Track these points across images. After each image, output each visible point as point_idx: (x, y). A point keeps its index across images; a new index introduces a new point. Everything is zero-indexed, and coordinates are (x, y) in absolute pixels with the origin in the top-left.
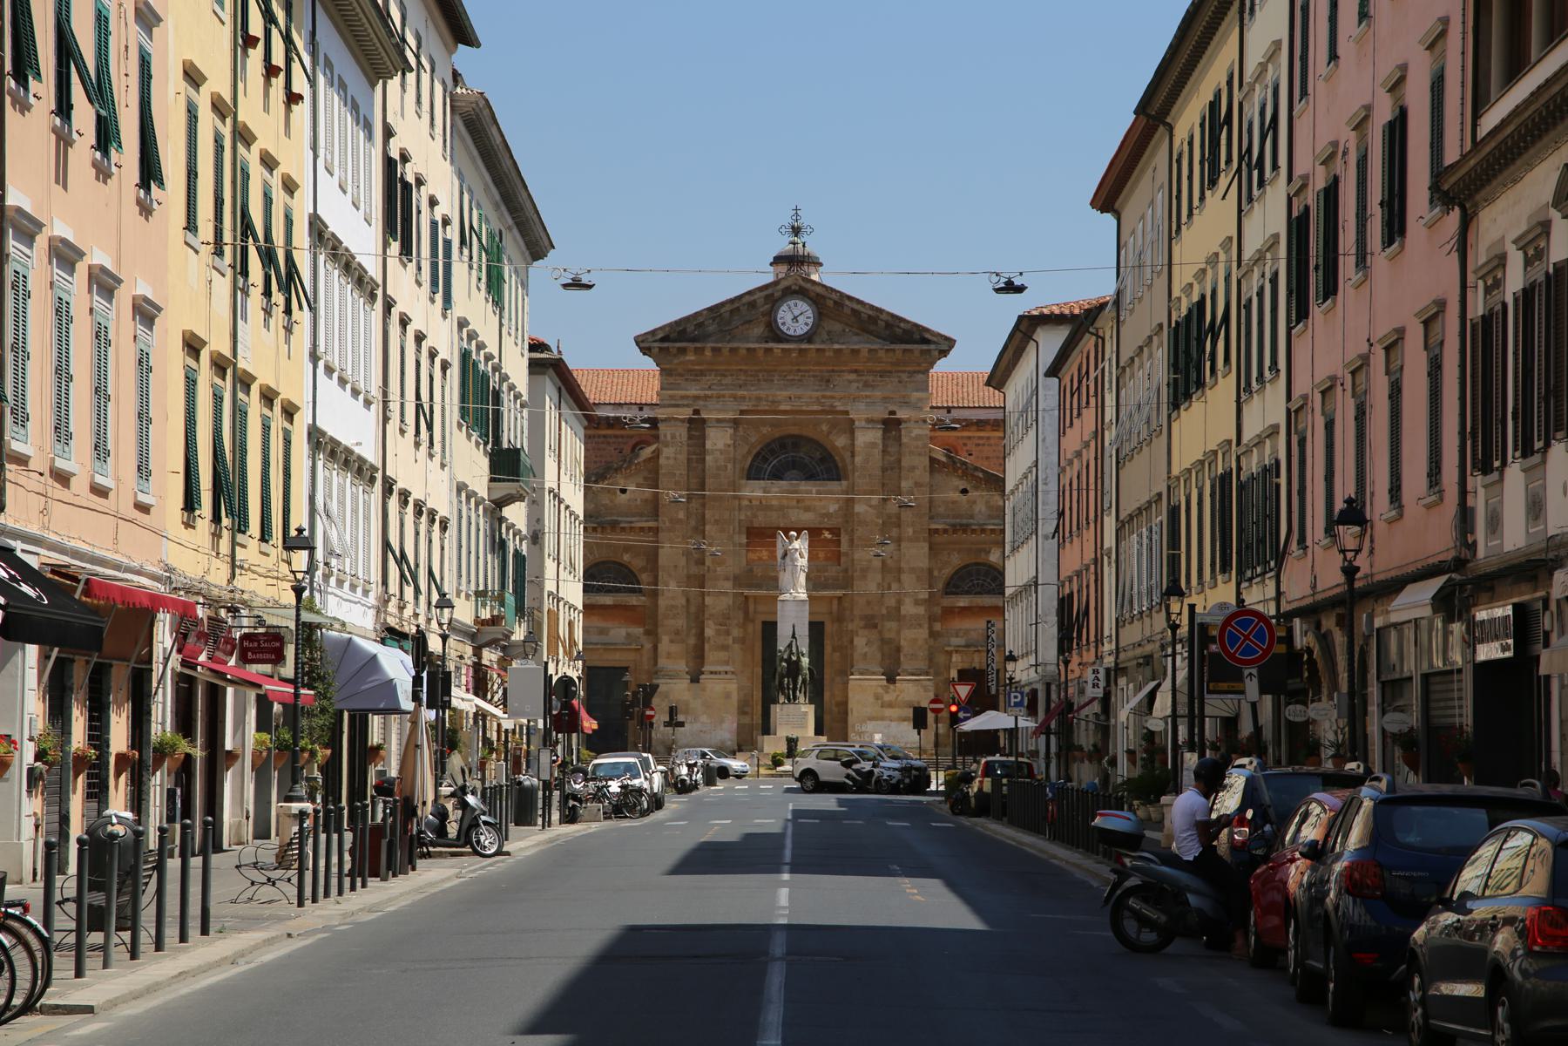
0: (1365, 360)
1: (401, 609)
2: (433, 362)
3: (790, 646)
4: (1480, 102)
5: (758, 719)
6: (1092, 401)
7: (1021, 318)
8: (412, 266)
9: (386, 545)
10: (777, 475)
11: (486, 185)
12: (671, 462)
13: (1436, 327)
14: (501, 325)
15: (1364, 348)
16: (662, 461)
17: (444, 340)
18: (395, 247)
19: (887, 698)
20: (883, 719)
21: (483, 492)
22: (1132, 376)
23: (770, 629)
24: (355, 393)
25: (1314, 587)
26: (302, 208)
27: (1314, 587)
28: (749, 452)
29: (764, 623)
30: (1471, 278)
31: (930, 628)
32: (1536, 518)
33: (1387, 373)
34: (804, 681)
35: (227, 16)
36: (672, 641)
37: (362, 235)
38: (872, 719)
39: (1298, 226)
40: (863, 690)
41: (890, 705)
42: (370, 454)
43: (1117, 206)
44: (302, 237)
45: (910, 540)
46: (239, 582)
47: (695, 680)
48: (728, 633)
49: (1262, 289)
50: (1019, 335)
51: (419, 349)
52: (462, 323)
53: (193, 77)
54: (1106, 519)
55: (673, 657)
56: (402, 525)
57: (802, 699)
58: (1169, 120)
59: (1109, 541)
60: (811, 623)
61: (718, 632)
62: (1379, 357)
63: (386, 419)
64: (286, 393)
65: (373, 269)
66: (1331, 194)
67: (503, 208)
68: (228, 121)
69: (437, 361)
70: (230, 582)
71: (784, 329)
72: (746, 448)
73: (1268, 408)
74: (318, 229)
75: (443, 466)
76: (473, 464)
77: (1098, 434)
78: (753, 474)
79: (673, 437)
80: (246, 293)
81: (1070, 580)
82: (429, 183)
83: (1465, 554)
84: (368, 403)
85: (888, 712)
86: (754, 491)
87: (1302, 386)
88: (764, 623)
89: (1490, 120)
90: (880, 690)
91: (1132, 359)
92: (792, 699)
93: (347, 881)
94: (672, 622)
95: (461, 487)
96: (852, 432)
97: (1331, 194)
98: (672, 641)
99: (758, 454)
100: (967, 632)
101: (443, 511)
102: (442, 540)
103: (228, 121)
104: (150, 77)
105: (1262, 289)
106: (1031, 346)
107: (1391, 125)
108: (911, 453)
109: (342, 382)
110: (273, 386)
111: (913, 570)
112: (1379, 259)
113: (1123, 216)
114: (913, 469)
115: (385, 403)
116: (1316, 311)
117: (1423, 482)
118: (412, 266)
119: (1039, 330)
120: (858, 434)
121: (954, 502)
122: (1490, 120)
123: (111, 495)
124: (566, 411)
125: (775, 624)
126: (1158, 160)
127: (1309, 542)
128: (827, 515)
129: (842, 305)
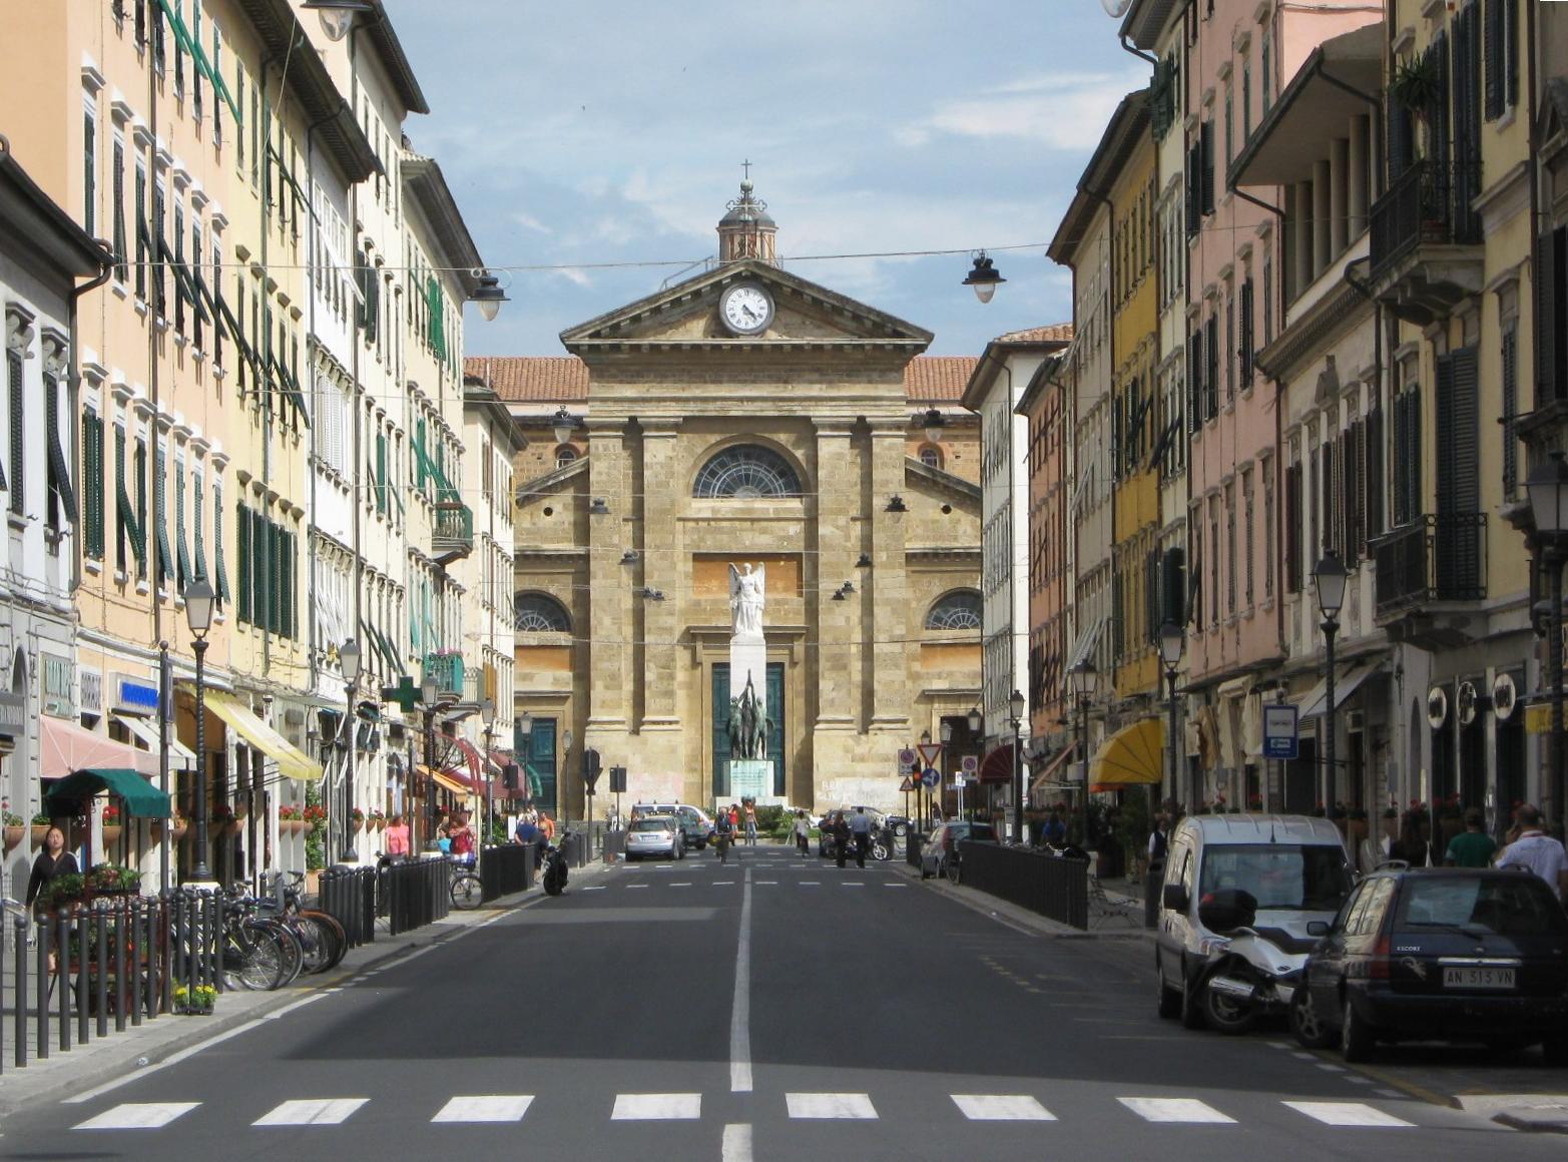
0: (1233, 478)
1: (370, 682)
2: (389, 433)
3: (745, 695)
4: (1287, 302)
5: (709, 777)
6: (1056, 449)
7: (990, 346)
8: (374, 346)
9: (359, 621)
10: (728, 491)
11: (428, 236)
12: (604, 477)
13: (1232, 490)
14: (441, 372)
15: (1231, 471)
16: (593, 477)
17: (398, 409)
18: (362, 332)
19: (859, 750)
20: (854, 775)
21: (430, 554)
22: (1087, 437)
23: (722, 670)
24: (337, 484)
25: (1206, 666)
26: (301, 329)
27: (1206, 666)
28: (695, 465)
29: (715, 665)
30: (1284, 437)
31: (908, 669)
32: (1356, 619)
33: (1264, 481)
34: (761, 734)
35: (259, 194)
36: (607, 687)
37: (337, 336)
38: (839, 775)
39: (1195, 341)
40: (831, 748)
41: (862, 759)
42: (348, 540)
43: (1073, 259)
44: (303, 353)
45: (884, 566)
46: (272, 675)
47: (636, 732)
48: (672, 677)
49: (1174, 389)
50: (988, 362)
51: (379, 420)
52: (411, 387)
53: (242, 254)
54: (1068, 574)
55: (610, 705)
56: (380, 608)
57: (760, 755)
58: (1109, 197)
59: (1071, 599)
60: (769, 665)
61: (660, 677)
62: (1240, 479)
63: (358, 501)
64: (296, 504)
65: (345, 360)
66: (1212, 324)
67: (442, 253)
68: (148, 149)
69: (393, 432)
70: (265, 673)
71: (734, 321)
72: (692, 461)
73: (1175, 506)
74: (313, 342)
75: (398, 534)
76: (419, 527)
77: (1061, 486)
78: (701, 488)
79: (606, 448)
80: (271, 422)
81: (1040, 631)
82: (365, 230)
83: (1285, 655)
84: (345, 491)
85: (859, 767)
86: (703, 507)
87: (1198, 491)
88: (715, 665)
89: (1297, 312)
90: (850, 742)
91: (1086, 419)
92: (749, 755)
93: (54, 1024)
94: (606, 665)
95: (412, 553)
96: (814, 441)
97: (1212, 324)
98: (607, 687)
99: (705, 467)
100: (950, 674)
101: (399, 582)
102: (398, 608)
103: (148, 149)
104: (122, 170)
105: (1174, 389)
106: (1004, 373)
107: (1244, 286)
108: (884, 464)
109: (329, 477)
110: (249, 471)
111: (887, 602)
112: (1240, 395)
113: (1078, 270)
114: (886, 483)
115: (357, 489)
116: (1206, 426)
117: (1499, 485)
118: (374, 346)
119: (1010, 357)
120: (821, 442)
121: (934, 522)
122: (1297, 312)
123: (100, 575)
124: (315, 154)
125: (727, 665)
126: (1101, 227)
127: (1203, 628)
128: (789, 538)
129: (801, 294)
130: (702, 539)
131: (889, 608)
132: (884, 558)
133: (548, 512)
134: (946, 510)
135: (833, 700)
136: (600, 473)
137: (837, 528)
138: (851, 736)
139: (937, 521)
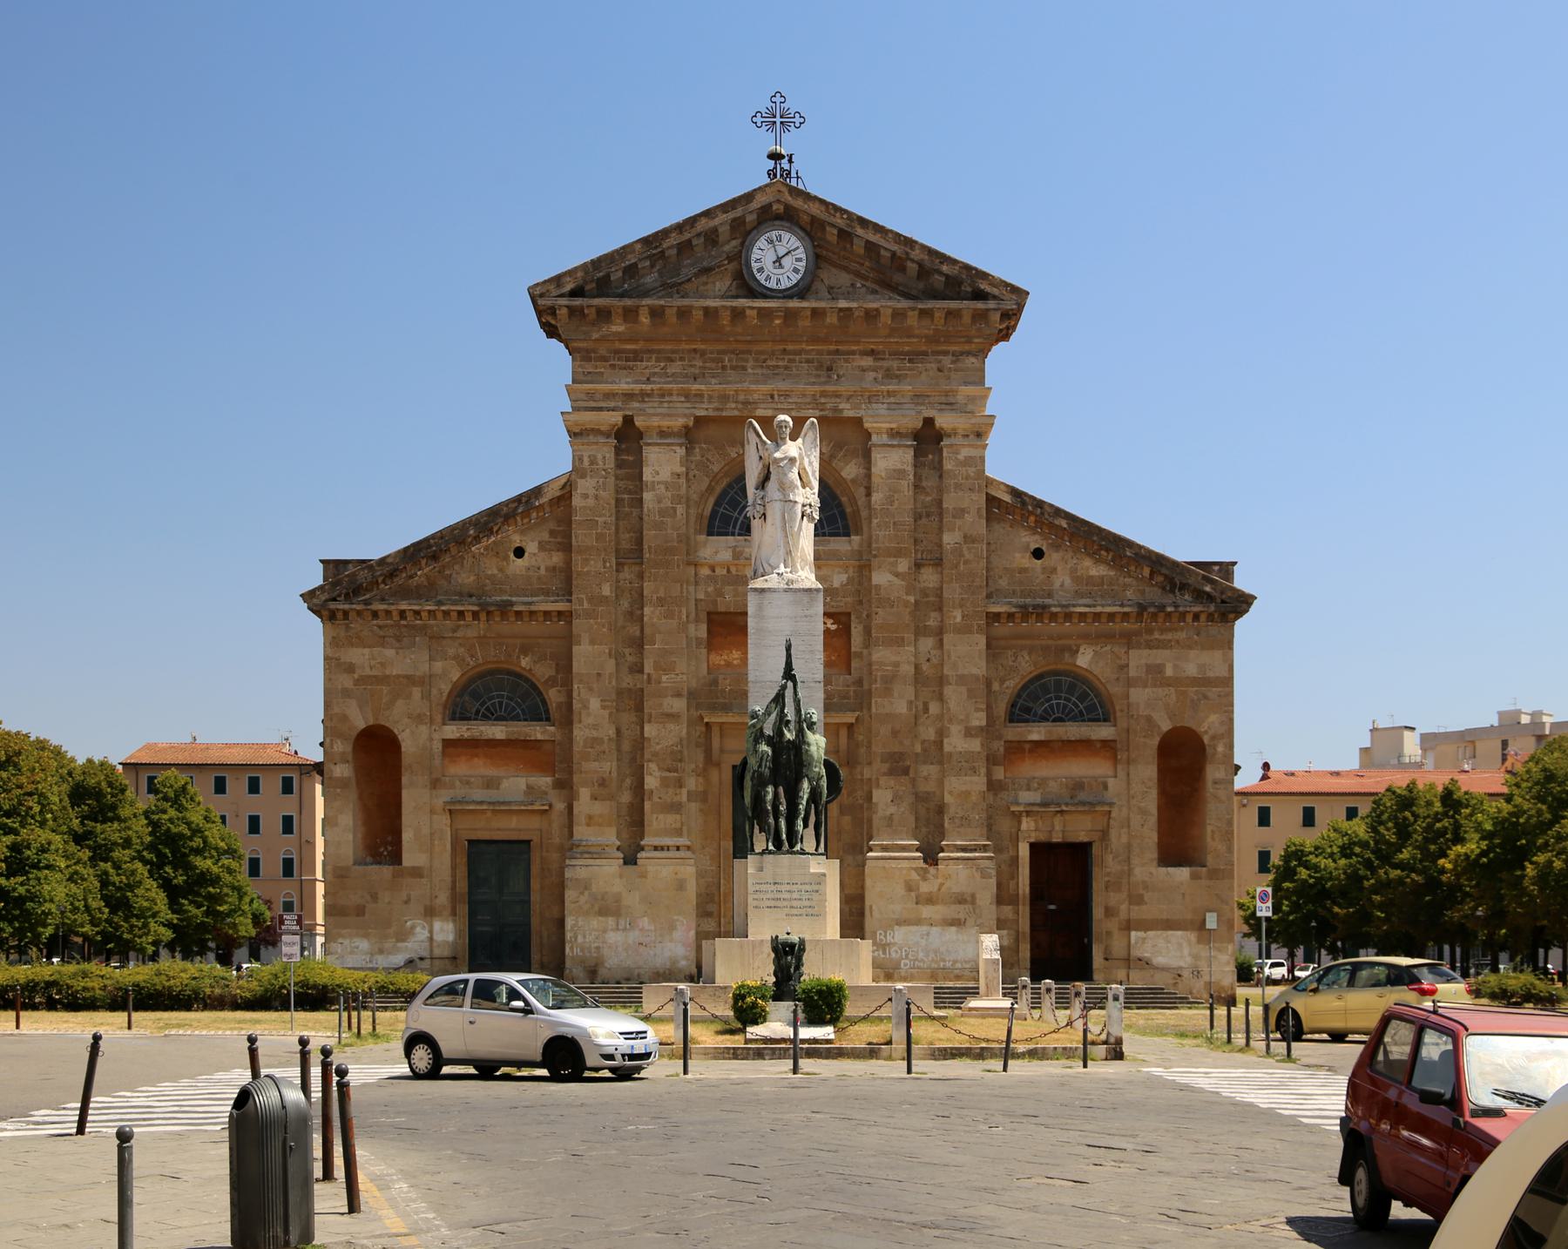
19: (925, 888)
20: (918, 922)
41: (930, 900)
85: (927, 911)
90: (914, 876)
100: (1043, 782)
108: (958, 486)
130: (720, 594)
131: (963, 689)
132: (959, 619)
133: (519, 552)
134: (1038, 554)
135: (891, 818)
136: (586, 496)
137: (897, 575)
138: (915, 869)
139: (1023, 570)
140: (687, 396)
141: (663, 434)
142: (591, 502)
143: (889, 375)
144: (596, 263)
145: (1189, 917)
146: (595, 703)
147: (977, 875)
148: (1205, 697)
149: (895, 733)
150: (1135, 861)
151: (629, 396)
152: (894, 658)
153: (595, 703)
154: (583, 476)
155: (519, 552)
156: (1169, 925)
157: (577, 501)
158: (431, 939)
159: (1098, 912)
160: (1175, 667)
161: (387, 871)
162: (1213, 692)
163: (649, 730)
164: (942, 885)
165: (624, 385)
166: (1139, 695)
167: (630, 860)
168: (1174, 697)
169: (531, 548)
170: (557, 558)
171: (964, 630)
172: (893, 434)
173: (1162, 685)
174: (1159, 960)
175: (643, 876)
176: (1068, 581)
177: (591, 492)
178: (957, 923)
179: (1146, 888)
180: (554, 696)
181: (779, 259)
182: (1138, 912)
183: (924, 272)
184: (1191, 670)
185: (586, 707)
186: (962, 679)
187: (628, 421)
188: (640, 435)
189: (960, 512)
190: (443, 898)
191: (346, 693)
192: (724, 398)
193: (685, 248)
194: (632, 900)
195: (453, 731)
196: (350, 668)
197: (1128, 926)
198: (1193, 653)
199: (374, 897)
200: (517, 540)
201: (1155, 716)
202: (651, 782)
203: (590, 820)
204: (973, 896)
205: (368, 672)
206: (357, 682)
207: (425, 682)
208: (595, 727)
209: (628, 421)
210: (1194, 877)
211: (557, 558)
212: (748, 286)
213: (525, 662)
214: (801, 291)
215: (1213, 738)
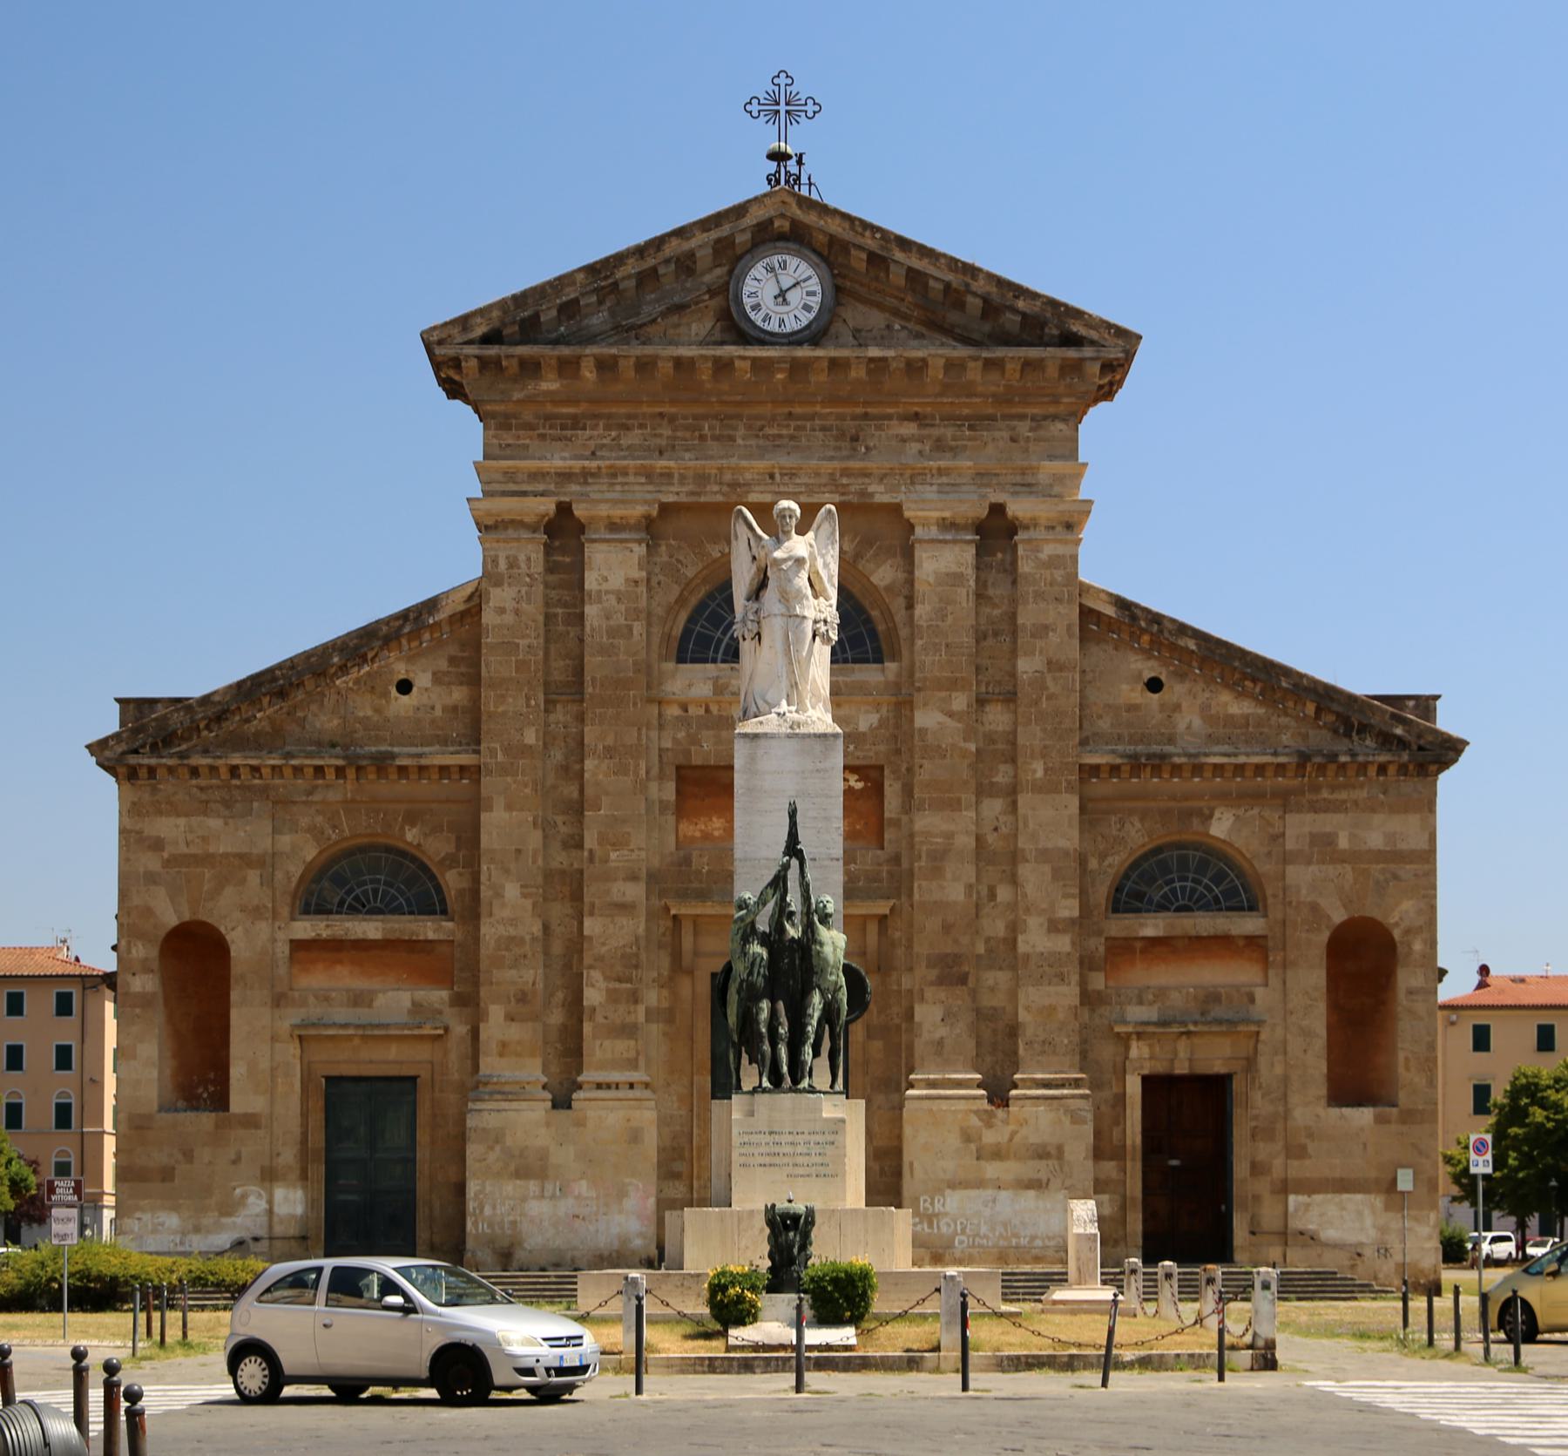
19: (989, 1138)
20: (980, 1184)
31: (1083, 983)
41: (997, 1154)
85: (992, 1170)
90: (975, 1121)
100: (1161, 993)
108: (1039, 595)
131: (1047, 868)
132: (1040, 774)
134: (1154, 685)
135: (940, 1043)
136: (502, 611)
137: (951, 715)
140: (649, 475)
141: (613, 526)
142: (509, 618)
143: (940, 446)
144: (520, 299)
145: (1373, 1174)
146: (512, 891)
147: (1066, 1121)
148: (1396, 877)
149: (947, 928)
150: (1294, 1099)
151: (565, 476)
152: (945, 827)
153: (512, 891)
154: (498, 583)
155: (405, 687)
156: (1343, 1186)
157: (488, 617)
158: (270, 1212)
159: (1240, 1169)
160: (1352, 837)
161: (207, 1120)
162: (1406, 871)
163: (591, 926)
164: (1013, 1134)
165: (558, 461)
166: (1301, 876)
167: (562, 1102)
168: (1350, 876)
169: (422, 680)
170: (459, 695)
171: (1047, 788)
172: (947, 525)
173: (1333, 861)
174: (1330, 1234)
175: (581, 1123)
176: (1197, 722)
177: (510, 605)
178: (1036, 1185)
179: (1310, 1135)
180: (452, 881)
181: (782, 293)
182: (1297, 1169)
183: (990, 309)
184: (1375, 840)
185: (499, 894)
186: (1044, 855)
187: (564, 509)
188: (581, 528)
189: (1042, 630)
190: (288, 1156)
191: (151, 878)
192: (702, 479)
193: (647, 278)
194: (565, 1157)
195: (305, 929)
196: (157, 845)
197: (1284, 1188)
198: (1377, 819)
199: (188, 1155)
200: (401, 671)
201: (1323, 902)
202: (593, 996)
203: (504, 1048)
204: (1060, 1149)
205: (184, 849)
206: (167, 863)
207: (265, 863)
208: (513, 922)
209: (564, 509)
210: (1380, 1120)
211: (459, 695)
212: (737, 329)
213: (411, 835)
214: (814, 335)
215: (1408, 932)
